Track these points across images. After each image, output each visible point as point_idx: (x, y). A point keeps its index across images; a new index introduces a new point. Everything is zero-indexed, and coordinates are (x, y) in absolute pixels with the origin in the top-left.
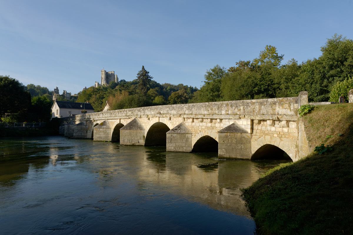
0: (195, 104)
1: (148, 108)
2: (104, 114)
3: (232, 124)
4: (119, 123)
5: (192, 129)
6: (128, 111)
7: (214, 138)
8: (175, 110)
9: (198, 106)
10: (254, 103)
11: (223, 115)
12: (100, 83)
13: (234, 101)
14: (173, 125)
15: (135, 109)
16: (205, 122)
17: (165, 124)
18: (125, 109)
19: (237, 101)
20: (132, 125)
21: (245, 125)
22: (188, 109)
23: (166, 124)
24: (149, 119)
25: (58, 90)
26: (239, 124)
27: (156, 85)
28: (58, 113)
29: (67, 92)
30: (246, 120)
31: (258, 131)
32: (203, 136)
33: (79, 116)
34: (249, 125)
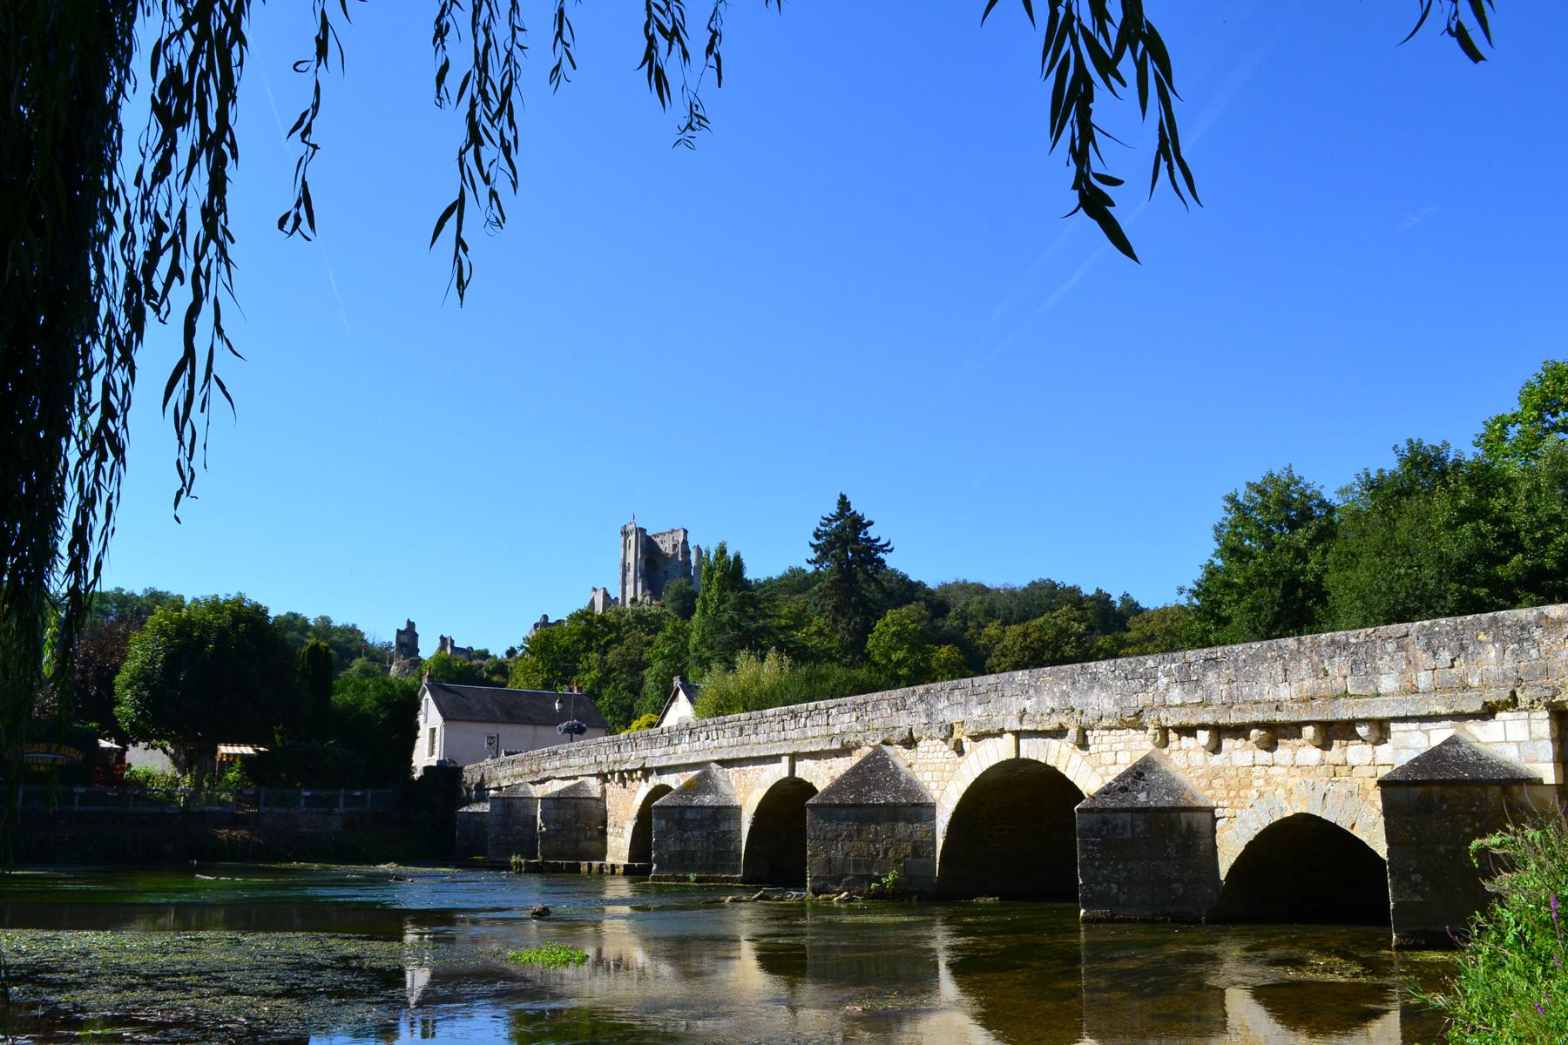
0: (1218, 651)
3: (1445, 743)
4: (786, 774)
5: (1210, 786)
6: (834, 711)
7: (1345, 825)
9: (1236, 660)
12: (615, 593)
13: (1443, 621)
14: (1101, 770)
15: (878, 695)
16: (1206, 760)
17: (1054, 769)
18: (822, 704)
19: (1459, 619)
20: (865, 782)
21: (1518, 743)
22: (1184, 679)
23: (1061, 769)
24: (960, 750)
25: (417, 635)
26: (1484, 738)
27: (909, 590)
29: (456, 645)
30: (1525, 714)
32: (1277, 818)
33: (560, 751)
34: (1541, 739)
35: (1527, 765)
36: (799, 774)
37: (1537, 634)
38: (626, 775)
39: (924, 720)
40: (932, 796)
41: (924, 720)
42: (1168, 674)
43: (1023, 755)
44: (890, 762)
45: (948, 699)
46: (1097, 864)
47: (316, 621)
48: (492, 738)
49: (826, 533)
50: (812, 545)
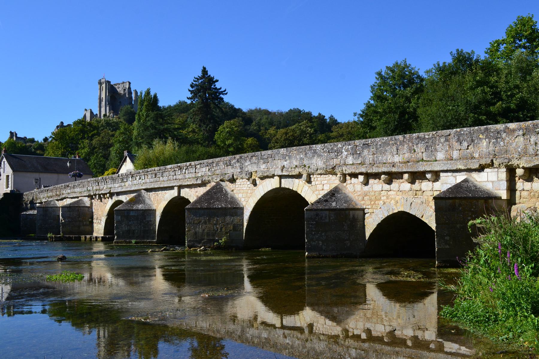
0: (369, 141)
1: (252, 157)
2: (138, 178)
3: (462, 182)
4: (176, 195)
8: (319, 156)
9: (377, 145)
10: (514, 131)
11: (439, 161)
12: (96, 111)
14: (317, 192)
15: (217, 159)
17: (296, 192)
19: (472, 128)
20: (212, 198)
21: (493, 182)
22: (354, 153)
23: (299, 192)
24: (255, 184)
26: (479, 180)
27: (234, 113)
28: (10, 183)
29: (18, 136)
30: (496, 170)
31: (524, 194)
32: (391, 213)
33: (70, 185)
34: (502, 180)
35: (495, 191)
36: (182, 194)
40: (242, 204)
42: (347, 151)
43: (283, 186)
44: (224, 189)
45: (250, 161)
46: (313, 233)
49: (196, 85)
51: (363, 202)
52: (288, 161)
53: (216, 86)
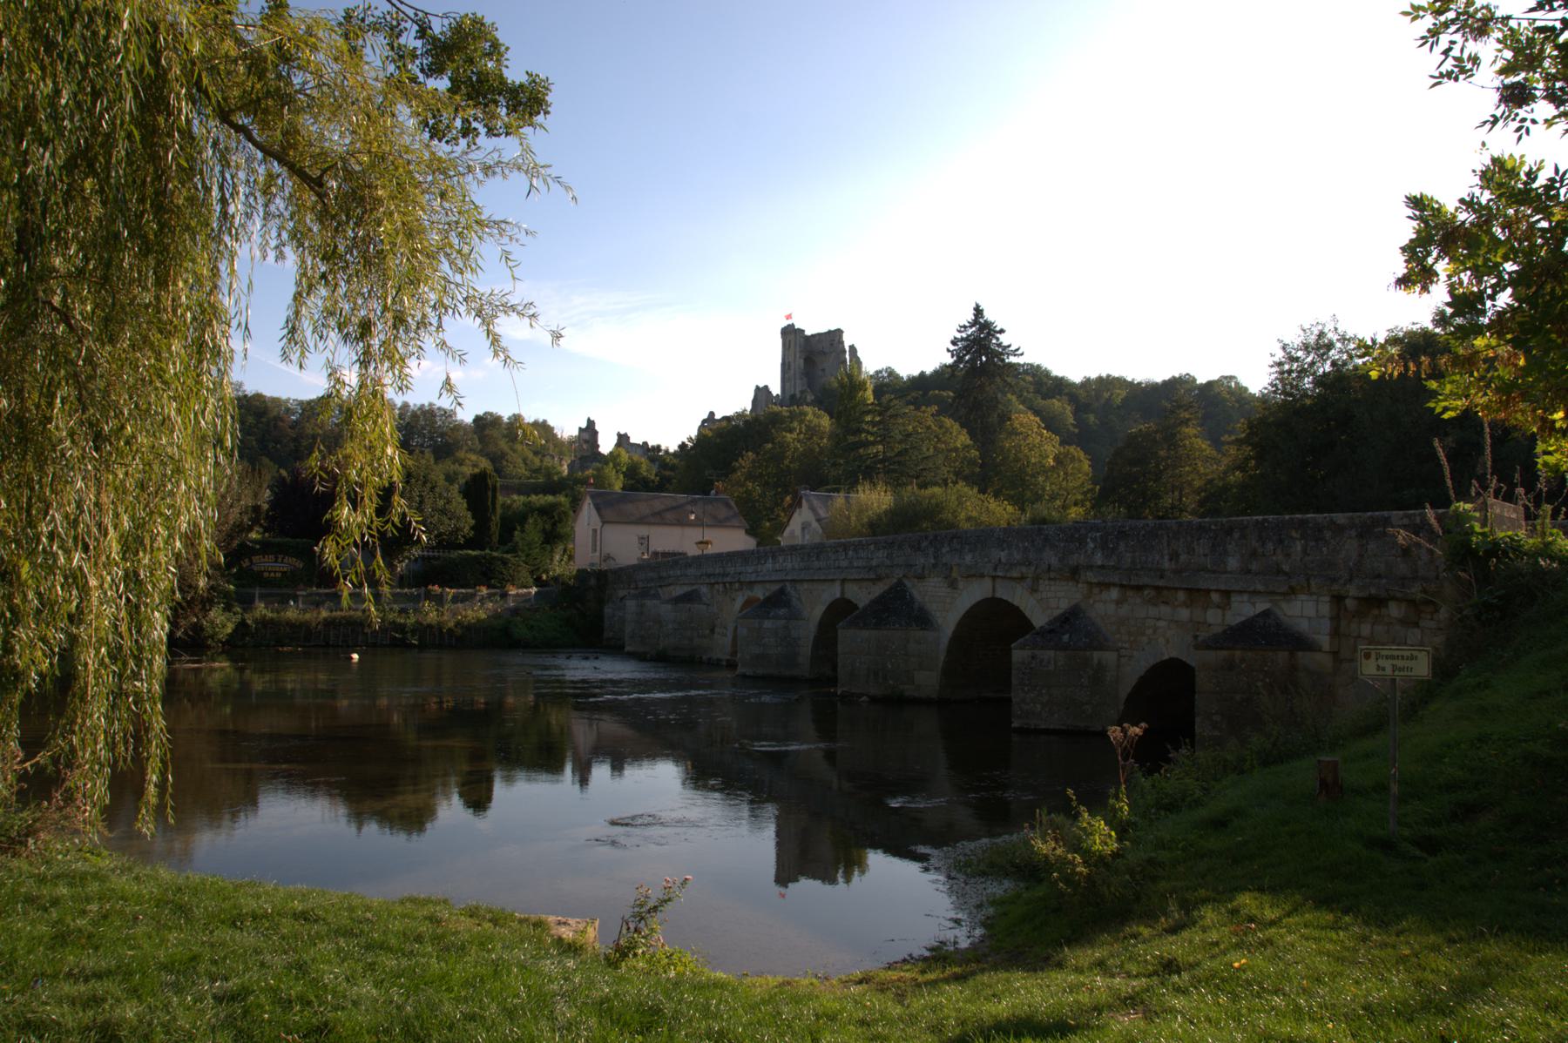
4: (838, 595)
17: (1018, 608)
21: (1310, 618)
23: (1022, 608)
25: (596, 433)
32: (1158, 661)
34: (1324, 617)
35: (1314, 636)
36: (848, 596)
37: (1328, 534)
38: (727, 585)
39: (933, 561)
41: (933, 561)
42: (1094, 540)
43: (998, 595)
46: (1026, 689)
47: (509, 418)
48: (643, 538)
49: (962, 339)
50: (948, 350)
51: (1118, 636)
52: (1006, 552)
53: (1001, 340)
